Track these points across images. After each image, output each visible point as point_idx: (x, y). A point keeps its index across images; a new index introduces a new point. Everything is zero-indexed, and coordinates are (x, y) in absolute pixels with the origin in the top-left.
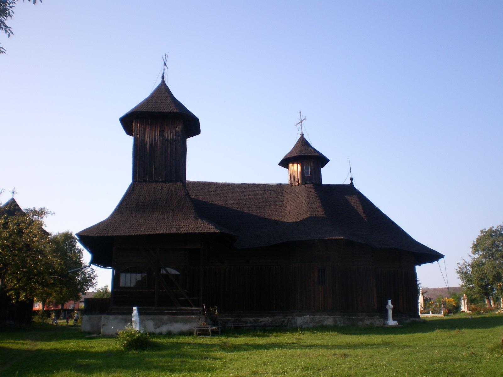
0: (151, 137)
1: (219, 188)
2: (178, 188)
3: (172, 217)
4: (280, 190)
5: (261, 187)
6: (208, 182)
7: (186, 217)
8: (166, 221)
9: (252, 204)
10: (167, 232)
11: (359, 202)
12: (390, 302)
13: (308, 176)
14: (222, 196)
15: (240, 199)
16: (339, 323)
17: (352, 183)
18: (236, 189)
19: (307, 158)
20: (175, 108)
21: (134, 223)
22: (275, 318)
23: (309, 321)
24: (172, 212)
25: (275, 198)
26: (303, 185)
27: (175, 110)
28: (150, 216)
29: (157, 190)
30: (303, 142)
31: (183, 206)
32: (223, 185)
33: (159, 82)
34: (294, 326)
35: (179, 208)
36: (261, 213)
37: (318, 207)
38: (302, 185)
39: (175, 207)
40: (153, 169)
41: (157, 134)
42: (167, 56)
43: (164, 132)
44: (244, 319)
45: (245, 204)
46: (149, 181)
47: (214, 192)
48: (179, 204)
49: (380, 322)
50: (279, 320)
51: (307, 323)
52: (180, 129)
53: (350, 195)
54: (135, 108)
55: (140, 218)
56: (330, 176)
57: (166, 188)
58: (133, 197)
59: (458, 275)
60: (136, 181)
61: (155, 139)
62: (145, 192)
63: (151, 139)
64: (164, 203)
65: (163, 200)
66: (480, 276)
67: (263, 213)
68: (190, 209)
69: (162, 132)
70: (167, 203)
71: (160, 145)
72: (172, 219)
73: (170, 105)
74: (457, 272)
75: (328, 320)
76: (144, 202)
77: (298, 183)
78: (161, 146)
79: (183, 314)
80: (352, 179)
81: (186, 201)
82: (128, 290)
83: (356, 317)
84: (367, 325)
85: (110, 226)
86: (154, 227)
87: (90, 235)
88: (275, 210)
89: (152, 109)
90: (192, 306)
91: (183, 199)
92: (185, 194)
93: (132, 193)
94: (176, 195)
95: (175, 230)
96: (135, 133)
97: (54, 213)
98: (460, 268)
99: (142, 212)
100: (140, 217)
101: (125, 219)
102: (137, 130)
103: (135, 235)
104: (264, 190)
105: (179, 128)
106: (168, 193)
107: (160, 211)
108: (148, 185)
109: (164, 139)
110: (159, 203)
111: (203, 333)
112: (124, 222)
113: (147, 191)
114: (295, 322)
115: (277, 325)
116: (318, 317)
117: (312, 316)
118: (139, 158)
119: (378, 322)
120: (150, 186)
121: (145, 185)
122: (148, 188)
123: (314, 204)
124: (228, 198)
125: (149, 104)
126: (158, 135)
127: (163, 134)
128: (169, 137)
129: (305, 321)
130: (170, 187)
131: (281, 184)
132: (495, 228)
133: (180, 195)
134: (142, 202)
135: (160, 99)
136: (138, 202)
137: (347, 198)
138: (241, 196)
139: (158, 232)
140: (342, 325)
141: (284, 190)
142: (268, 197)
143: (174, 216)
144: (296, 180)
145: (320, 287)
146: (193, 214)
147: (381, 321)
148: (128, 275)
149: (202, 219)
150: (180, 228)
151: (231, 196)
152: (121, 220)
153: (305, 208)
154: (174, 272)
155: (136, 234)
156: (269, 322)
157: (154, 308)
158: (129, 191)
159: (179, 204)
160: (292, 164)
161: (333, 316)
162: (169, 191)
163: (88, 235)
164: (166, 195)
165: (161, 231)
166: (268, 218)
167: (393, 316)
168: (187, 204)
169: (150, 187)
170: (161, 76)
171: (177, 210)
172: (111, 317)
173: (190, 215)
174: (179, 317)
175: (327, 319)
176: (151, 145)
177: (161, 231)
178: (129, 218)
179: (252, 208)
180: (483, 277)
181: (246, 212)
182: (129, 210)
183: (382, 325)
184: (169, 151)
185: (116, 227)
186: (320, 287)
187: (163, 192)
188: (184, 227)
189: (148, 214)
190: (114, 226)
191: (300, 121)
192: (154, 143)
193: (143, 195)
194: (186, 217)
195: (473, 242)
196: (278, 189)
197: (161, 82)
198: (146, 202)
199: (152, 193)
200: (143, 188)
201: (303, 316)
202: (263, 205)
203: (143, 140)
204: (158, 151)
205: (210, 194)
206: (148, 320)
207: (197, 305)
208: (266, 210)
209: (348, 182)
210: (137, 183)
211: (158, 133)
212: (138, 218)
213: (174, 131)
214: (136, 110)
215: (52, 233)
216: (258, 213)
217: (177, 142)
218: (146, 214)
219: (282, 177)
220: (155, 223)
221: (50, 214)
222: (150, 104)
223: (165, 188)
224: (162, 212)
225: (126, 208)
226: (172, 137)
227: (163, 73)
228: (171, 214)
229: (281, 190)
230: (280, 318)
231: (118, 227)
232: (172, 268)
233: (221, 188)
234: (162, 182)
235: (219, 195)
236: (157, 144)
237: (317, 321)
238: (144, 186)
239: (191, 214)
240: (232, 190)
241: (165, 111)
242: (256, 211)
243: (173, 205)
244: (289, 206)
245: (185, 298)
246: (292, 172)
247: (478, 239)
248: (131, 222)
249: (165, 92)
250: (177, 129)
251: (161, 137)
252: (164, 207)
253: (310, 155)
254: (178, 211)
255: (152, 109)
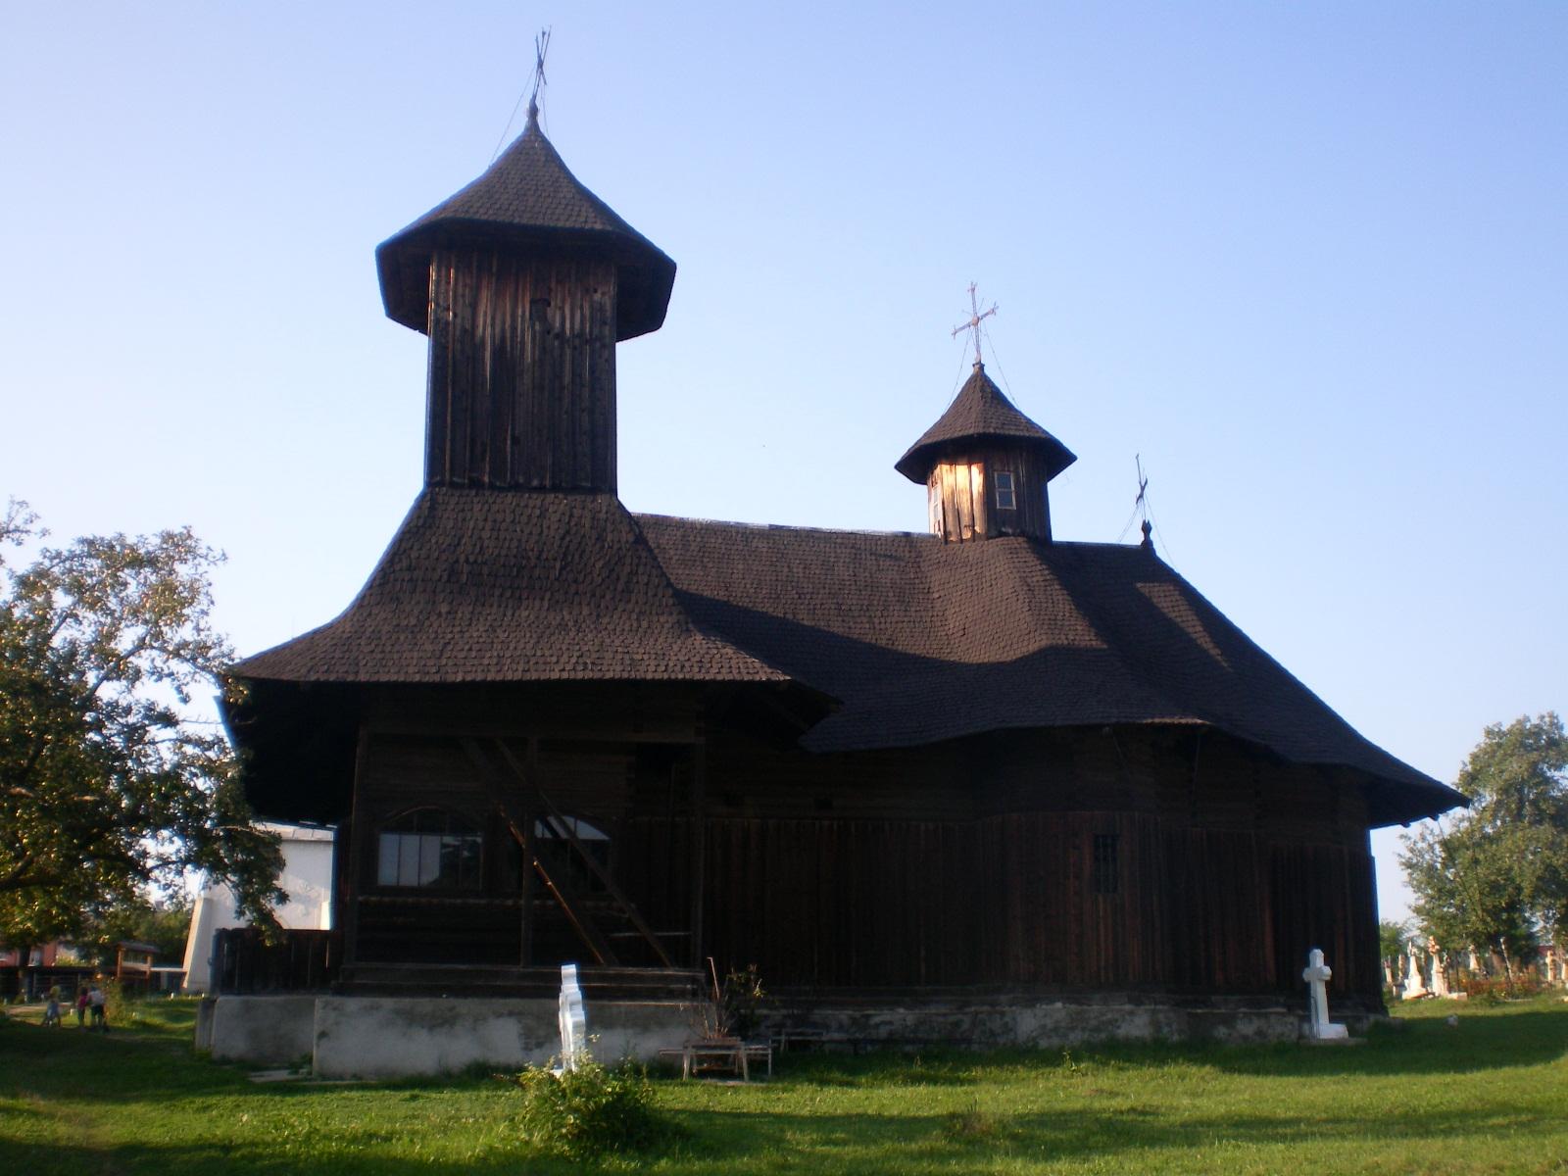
0: (498, 322)
1: (695, 537)
2: (603, 516)
3: (594, 623)
4: (907, 555)
5: (839, 541)
6: (652, 516)
7: (645, 624)
8: (572, 634)
9: (820, 596)
10: (589, 675)
11: (1187, 607)
12: (1318, 957)
13: (1008, 508)
14: (710, 565)
15: (774, 578)
16: (1166, 1030)
17: (1147, 544)
18: (754, 544)
19: (1002, 445)
20: (595, 217)
21: (450, 636)
22: (927, 1011)
23: (1063, 1024)
24: (589, 604)
25: (898, 581)
26: (992, 538)
27: (595, 222)
28: (509, 613)
29: (524, 519)
30: (982, 390)
31: (628, 582)
32: (707, 530)
33: (518, 128)
34: (1001, 1040)
35: (615, 589)
36: (862, 631)
37: (1067, 615)
38: (989, 537)
39: (600, 585)
40: (506, 440)
41: (524, 312)
42: (546, 36)
43: (549, 305)
44: (818, 1014)
45: (800, 598)
46: (492, 487)
47: (679, 552)
48: (614, 576)
49: (1290, 1027)
50: (941, 1019)
51: (1056, 1029)
52: (607, 297)
53: (1153, 582)
54: (444, 207)
55: (471, 619)
56: (1081, 511)
57: (558, 515)
58: (433, 541)
59: (1404, 875)
60: (441, 484)
61: (514, 328)
62: (481, 524)
63: (498, 330)
64: (554, 567)
65: (550, 557)
66: (1493, 878)
67: (867, 631)
68: (655, 595)
69: (540, 304)
70: (568, 569)
71: (533, 353)
72: (592, 627)
73: (573, 205)
74: (1403, 864)
75: (1132, 1021)
76: (479, 561)
77: (974, 531)
78: (537, 357)
79: (632, 995)
80: (1146, 528)
81: (637, 565)
82: (423, 900)
83: (1206, 1011)
84: (1245, 1038)
85: (360, 644)
86: (534, 655)
87: (285, 677)
88: (906, 619)
89: (510, 213)
90: (660, 964)
91: (625, 556)
92: (631, 538)
93: (430, 527)
94: (597, 539)
95: (619, 668)
96: (437, 304)
97: (224, 557)
98: (1412, 851)
99: (474, 599)
100: (468, 616)
101: (413, 621)
102: (447, 291)
103: (463, 683)
104: (854, 551)
105: (603, 294)
106: (568, 532)
107: (542, 599)
108: (491, 501)
109: (549, 333)
110: (536, 566)
111: (719, 1069)
112: (412, 632)
113: (486, 520)
114: (1008, 1029)
115: (935, 1036)
116: (1095, 1010)
117: (1073, 1007)
118: (453, 395)
119: (1279, 1025)
120: (494, 502)
121: (476, 500)
122: (489, 511)
123: (1050, 605)
124: (733, 573)
125: (497, 196)
126: (527, 314)
127: (545, 314)
128: (568, 325)
129: (1049, 1023)
130: (575, 510)
131: (907, 535)
132: (1535, 721)
133: (612, 541)
134: (471, 560)
135: (534, 182)
136: (457, 561)
137: (1143, 590)
138: (779, 569)
139: (552, 673)
140: (1176, 1038)
141: (925, 554)
142: (871, 577)
143: (598, 616)
144: (965, 520)
145: (1101, 899)
146: (671, 614)
147: (1292, 1024)
148: (411, 841)
149: (706, 633)
150: (632, 659)
151: (741, 567)
152: (398, 625)
153: (1022, 616)
154: (587, 832)
155: (469, 678)
156: (907, 1026)
157: (516, 969)
158: (419, 517)
159: (614, 576)
160: (951, 465)
161: (1147, 1007)
162: (572, 524)
163: (276, 677)
164: (563, 539)
165: (564, 670)
166: (890, 646)
167: (1331, 1008)
168: (643, 574)
169: (495, 508)
170: (527, 106)
171: (608, 597)
172: (352, 1004)
173: (657, 614)
174: (619, 1006)
175: (1127, 1017)
176: (499, 352)
177: (564, 670)
178: (428, 618)
179: (826, 612)
180: (1502, 882)
181: (806, 623)
182: (424, 591)
183: (1294, 1036)
184: (567, 379)
185: (383, 652)
186: (1101, 899)
187: (549, 528)
188: (646, 657)
189: (500, 606)
190: (373, 645)
191: (970, 319)
192: (512, 346)
193: (471, 537)
194: (645, 624)
195: (1461, 766)
196: (902, 549)
197: (527, 129)
198: (485, 563)
199: (507, 530)
200: (472, 510)
201: (1038, 1006)
202: (860, 602)
203: (469, 332)
204: (525, 377)
205: (667, 556)
206: (499, 1015)
207: (683, 958)
208: (876, 621)
209: (1135, 539)
210: (444, 489)
211: (524, 309)
212: (461, 618)
213: (586, 306)
214: (449, 214)
215: (224, 636)
216: (850, 628)
217: (598, 345)
218: (491, 606)
219: (911, 511)
220: (532, 641)
221: (206, 557)
222: (499, 199)
223: (555, 512)
224: (550, 600)
225: (411, 580)
226: (577, 326)
227: (535, 97)
228: (585, 612)
229: (913, 555)
230: (943, 1010)
231: (390, 652)
232: (580, 817)
233: (702, 538)
234: (541, 489)
235: (698, 563)
236: (523, 350)
237: (1094, 1023)
238: (472, 502)
239: (663, 613)
240: (741, 548)
241: (560, 224)
242: (843, 621)
243: (590, 577)
244: (957, 610)
245: (638, 934)
246: (947, 491)
247: (1475, 758)
248: (436, 632)
249: (546, 160)
250: (597, 297)
251: (537, 323)
252: (556, 583)
253: (1018, 433)
254: (613, 599)
255: (512, 215)
